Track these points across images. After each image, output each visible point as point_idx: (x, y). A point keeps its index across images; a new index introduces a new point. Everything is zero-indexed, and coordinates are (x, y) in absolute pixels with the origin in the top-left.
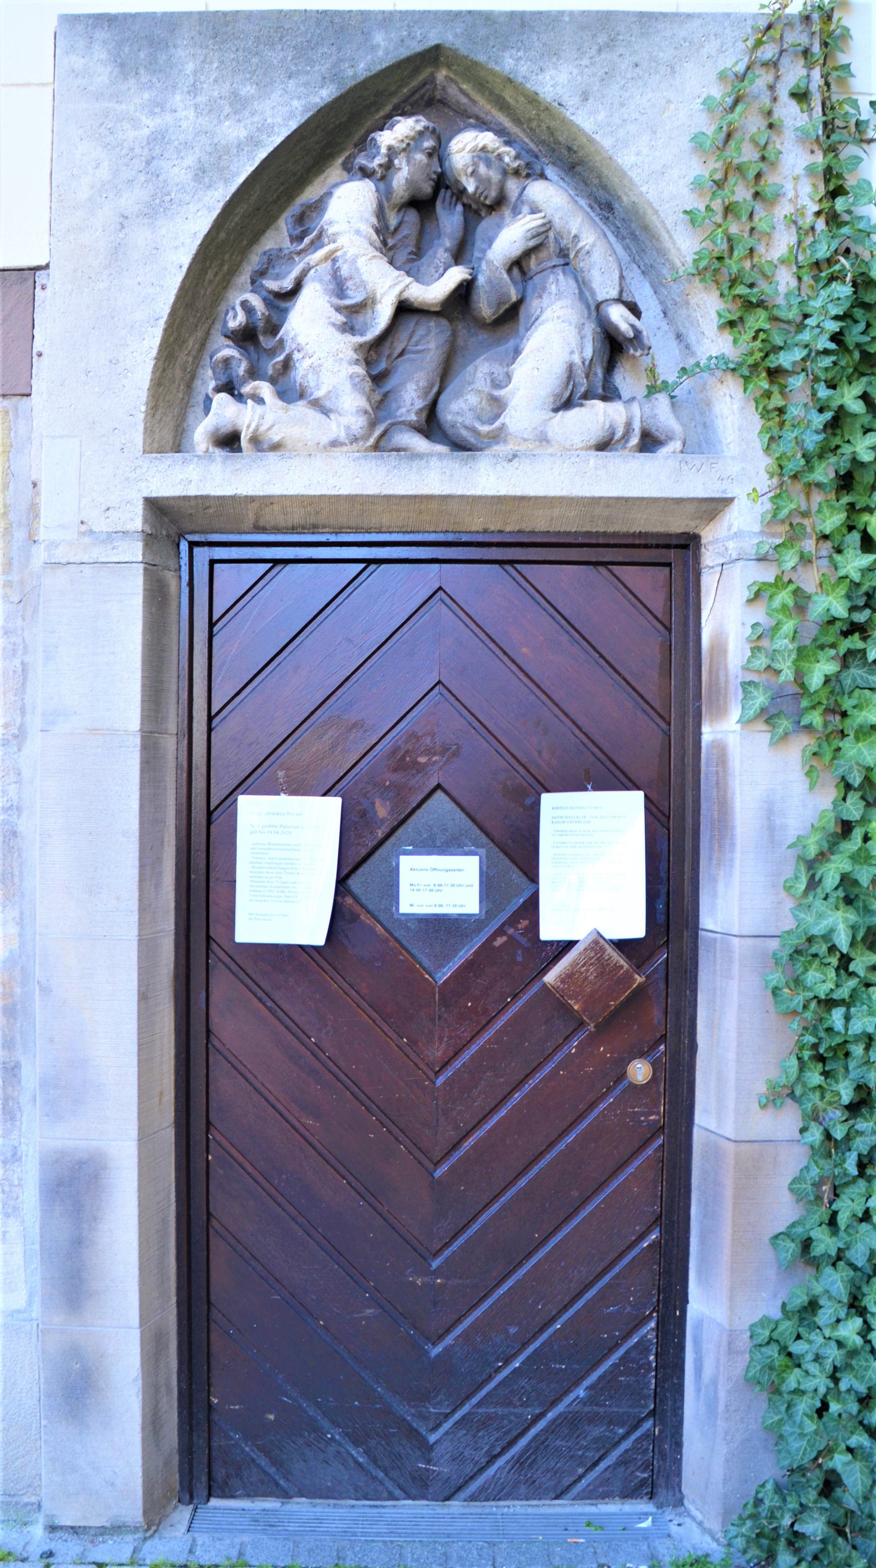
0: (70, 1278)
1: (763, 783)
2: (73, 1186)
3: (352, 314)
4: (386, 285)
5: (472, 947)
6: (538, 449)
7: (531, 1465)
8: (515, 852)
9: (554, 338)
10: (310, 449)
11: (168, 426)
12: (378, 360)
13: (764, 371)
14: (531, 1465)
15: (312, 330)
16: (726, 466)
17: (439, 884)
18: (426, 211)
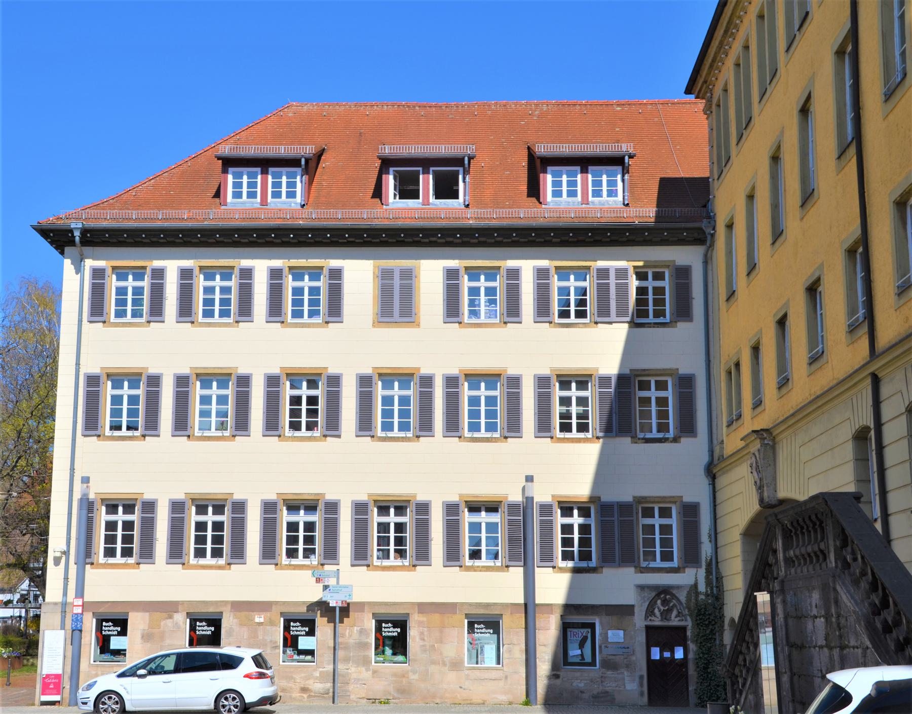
0: (641, 685)
1: (692, 647)
2: (641, 677)
3: (660, 611)
4: (662, 608)
5: (874, 484)
6: (675, 622)
7: (730, 373)
8: (673, 653)
9: (675, 613)
10: (657, 622)
11: (646, 619)
12: (662, 614)
13: (691, 616)
14: (730, 373)
15: (656, 611)
16: (689, 623)
17: (667, 655)
18: (664, 602)
